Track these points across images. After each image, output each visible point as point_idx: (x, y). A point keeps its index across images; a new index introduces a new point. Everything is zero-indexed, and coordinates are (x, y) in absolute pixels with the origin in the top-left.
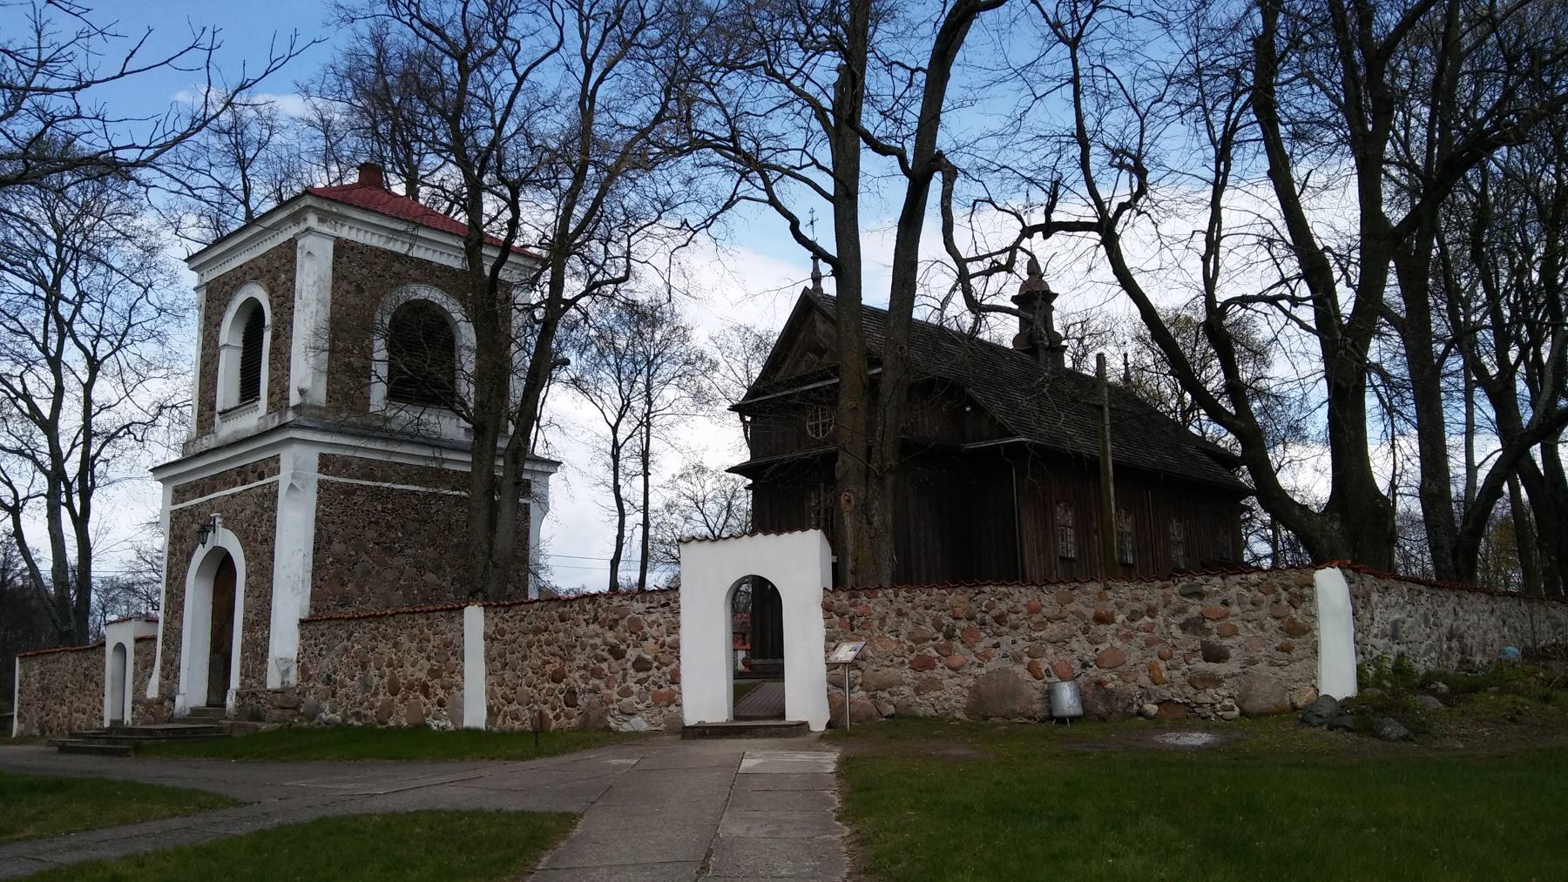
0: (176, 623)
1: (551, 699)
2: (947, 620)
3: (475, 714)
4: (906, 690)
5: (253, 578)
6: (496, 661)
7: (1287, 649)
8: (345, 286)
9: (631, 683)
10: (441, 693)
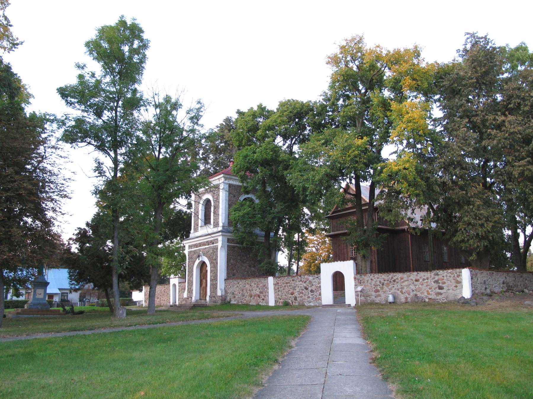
0: (191, 279)
1: (291, 299)
2: (382, 281)
3: (272, 303)
4: (373, 297)
5: (212, 269)
6: (276, 290)
7: (456, 287)
8: (231, 195)
9: (310, 295)
10: (263, 297)
